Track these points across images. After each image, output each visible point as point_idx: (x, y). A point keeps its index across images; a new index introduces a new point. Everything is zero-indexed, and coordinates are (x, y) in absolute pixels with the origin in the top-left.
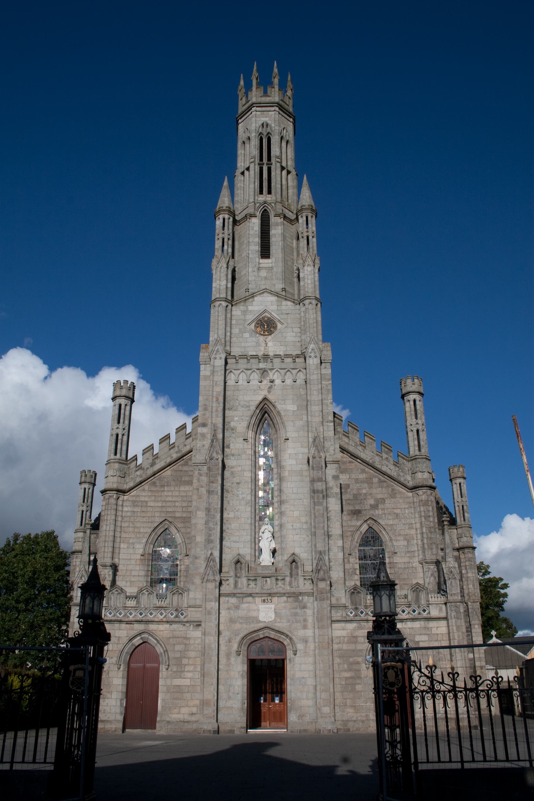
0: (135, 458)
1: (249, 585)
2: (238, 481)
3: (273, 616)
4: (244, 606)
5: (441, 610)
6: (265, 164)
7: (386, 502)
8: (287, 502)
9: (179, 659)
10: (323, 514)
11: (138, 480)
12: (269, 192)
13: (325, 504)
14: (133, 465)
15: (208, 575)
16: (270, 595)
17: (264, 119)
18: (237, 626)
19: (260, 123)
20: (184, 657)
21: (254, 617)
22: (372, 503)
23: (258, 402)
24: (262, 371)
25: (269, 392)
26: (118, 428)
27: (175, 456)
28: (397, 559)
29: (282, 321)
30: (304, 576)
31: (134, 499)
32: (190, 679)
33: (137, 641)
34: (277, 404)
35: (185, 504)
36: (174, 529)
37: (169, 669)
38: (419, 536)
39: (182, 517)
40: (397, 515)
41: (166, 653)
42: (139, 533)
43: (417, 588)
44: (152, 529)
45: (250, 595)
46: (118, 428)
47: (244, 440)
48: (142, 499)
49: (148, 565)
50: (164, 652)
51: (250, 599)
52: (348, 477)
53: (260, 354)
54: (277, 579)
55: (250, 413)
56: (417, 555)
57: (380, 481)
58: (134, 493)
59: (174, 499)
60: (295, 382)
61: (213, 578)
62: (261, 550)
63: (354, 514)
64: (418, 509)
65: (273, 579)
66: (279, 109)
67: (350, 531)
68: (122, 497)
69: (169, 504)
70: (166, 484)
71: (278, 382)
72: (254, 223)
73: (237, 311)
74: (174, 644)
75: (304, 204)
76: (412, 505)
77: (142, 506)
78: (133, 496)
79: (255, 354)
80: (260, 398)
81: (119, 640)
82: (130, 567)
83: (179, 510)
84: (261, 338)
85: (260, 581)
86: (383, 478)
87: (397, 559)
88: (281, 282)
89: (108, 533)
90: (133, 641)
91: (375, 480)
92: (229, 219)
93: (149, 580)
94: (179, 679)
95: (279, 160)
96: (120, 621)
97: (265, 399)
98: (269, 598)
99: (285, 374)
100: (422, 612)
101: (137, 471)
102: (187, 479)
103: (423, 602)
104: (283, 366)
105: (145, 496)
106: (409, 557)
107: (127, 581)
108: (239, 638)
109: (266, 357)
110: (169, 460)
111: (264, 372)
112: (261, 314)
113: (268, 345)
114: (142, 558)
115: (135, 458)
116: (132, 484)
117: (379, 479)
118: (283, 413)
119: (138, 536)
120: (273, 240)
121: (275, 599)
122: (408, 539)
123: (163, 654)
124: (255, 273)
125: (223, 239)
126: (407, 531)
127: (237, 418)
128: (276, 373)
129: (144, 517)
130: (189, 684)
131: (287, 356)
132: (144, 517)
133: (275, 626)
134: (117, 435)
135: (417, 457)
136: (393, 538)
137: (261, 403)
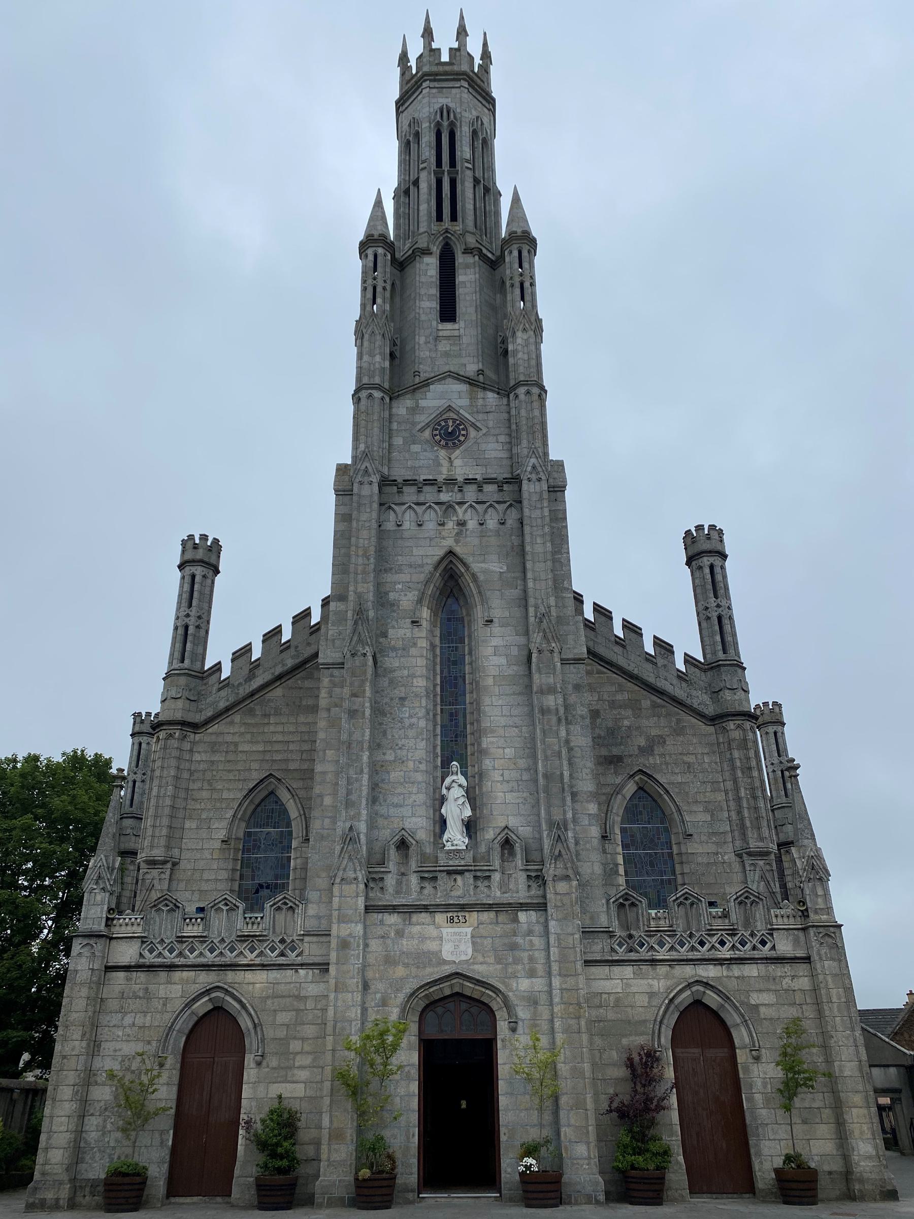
0: (218, 667)
1: (422, 888)
2: (403, 695)
3: (470, 951)
4: (416, 929)
5: (796, 942)
6: (446, 173)
7: (667, 743)
8: (492, 731)
9: (284, 1042)
10: (560, 753)
11: (222, 705)
12: (454, 218)
13: (563, 733)
14: (213, 679)
15: (344, 870)
16: (463, 907)
17: (443, 101)
18: (400, 971)
19: (437, 106)
20: (295, 1038)
21: (433, 953)
22: (642, 744)
23: (436, 558)
24: (444, 507)
25: (457, 541)
26: (188, 616)
27: (290, 663)
28: (692, 847)
29: (478, 424)
30: (527, 870)
31: (213, 738)
32: (305, 1083)
33: (202, 1006)
34: (469, 560)
35: (306, 747)
36: (285, 792)
37: (264, 1064)
38: (732, 804)
39: (301, 770)
40: (689, 765)
41: (258, 1029)
42: (221, 800)
43: (746, 898)
44: (245, 792)
45: (425, 908)
46: (188, 616)
47: (413, 622)
48: (229, 738)
49: (235, 860)
50: (255, 1026)
51: (424, 917)
52: (596, 698)
53: (440, 478)
54: (476, 878)
55: (422, 577)
56: (730, 840)
57: (654, 706)
58: (214, 728)
59: (286, 739)
60: (503, 523)
61: (353, 876)
62: (445, 822)
63: (611, 763)
64: (728, 756)
65: (469, 876)
66: (469, 84)
67: (604, 794)
68: (192, 735)
69: (277, 747)
70: (272, 712)
71: (472, 524)
72: (428, 264)
73: (401, 408)
74: (275, 1011)
75: (514, 229)
76: (715, 748)
77: (227, 752)
78: (211, 734)
79: (431, 478)
80: (441, 552)
81: (165, 1005)
82: (201, 865)
83: (294, 757)
84: (443, 453)
85: (443, 879)
86: (659, 701)
87: (692, 847)
88: (476, 360)
89: (161, 802)
90: (194, 1007)
91: (646, 703)
92: (385, 255)
93: (236, 888)
94: (284, 1085)
95: (470, 166)
96: (171, 967)
97: (451, 553)
98: (460, 914)
99: (486, 511)
100: (760, 946)
101: (220, 689)
102: (310, 702)
103: (760, 927)
104: (482, 498)
105: (233, 734)
106: (717, 844)
107: (193, 891)
108: (401, 997)
109: (451, 482)
110: (279, 670)
111: (449, 507)
112: (441, 414)
113: (454, 464)
114: (224, 846)
115: (218, 667)
116: (209, 713)
117: (653, 701)
118: (481, 577)
119: (218, 805)
120: (460, 291)
121: (473, 917)
122: (711, 809)
123: (253, 1031)
124: (431, 346)
125: (375, 288)
126: (710, 796)
127: (400, 586)
128: (469, 510)
129: (229, 771)
130: (302, 1095)
131: (489, 481)
132: (229, 771)
133: (473, 971)
134: (186, 627)
135: (721, 662)
136: (685, 808)
137: (442, 559)
